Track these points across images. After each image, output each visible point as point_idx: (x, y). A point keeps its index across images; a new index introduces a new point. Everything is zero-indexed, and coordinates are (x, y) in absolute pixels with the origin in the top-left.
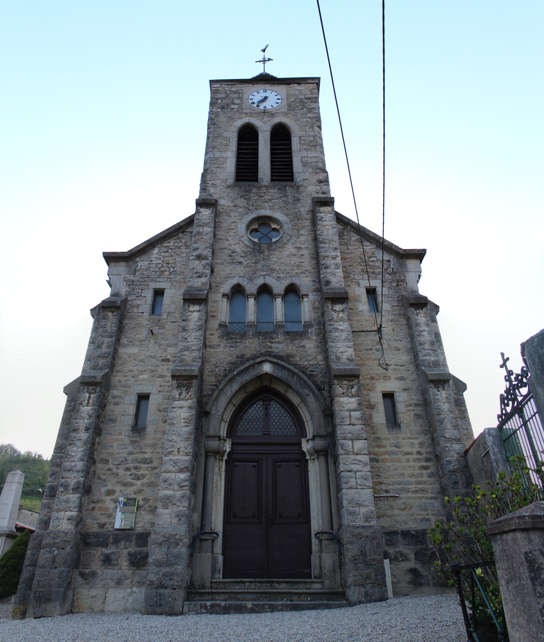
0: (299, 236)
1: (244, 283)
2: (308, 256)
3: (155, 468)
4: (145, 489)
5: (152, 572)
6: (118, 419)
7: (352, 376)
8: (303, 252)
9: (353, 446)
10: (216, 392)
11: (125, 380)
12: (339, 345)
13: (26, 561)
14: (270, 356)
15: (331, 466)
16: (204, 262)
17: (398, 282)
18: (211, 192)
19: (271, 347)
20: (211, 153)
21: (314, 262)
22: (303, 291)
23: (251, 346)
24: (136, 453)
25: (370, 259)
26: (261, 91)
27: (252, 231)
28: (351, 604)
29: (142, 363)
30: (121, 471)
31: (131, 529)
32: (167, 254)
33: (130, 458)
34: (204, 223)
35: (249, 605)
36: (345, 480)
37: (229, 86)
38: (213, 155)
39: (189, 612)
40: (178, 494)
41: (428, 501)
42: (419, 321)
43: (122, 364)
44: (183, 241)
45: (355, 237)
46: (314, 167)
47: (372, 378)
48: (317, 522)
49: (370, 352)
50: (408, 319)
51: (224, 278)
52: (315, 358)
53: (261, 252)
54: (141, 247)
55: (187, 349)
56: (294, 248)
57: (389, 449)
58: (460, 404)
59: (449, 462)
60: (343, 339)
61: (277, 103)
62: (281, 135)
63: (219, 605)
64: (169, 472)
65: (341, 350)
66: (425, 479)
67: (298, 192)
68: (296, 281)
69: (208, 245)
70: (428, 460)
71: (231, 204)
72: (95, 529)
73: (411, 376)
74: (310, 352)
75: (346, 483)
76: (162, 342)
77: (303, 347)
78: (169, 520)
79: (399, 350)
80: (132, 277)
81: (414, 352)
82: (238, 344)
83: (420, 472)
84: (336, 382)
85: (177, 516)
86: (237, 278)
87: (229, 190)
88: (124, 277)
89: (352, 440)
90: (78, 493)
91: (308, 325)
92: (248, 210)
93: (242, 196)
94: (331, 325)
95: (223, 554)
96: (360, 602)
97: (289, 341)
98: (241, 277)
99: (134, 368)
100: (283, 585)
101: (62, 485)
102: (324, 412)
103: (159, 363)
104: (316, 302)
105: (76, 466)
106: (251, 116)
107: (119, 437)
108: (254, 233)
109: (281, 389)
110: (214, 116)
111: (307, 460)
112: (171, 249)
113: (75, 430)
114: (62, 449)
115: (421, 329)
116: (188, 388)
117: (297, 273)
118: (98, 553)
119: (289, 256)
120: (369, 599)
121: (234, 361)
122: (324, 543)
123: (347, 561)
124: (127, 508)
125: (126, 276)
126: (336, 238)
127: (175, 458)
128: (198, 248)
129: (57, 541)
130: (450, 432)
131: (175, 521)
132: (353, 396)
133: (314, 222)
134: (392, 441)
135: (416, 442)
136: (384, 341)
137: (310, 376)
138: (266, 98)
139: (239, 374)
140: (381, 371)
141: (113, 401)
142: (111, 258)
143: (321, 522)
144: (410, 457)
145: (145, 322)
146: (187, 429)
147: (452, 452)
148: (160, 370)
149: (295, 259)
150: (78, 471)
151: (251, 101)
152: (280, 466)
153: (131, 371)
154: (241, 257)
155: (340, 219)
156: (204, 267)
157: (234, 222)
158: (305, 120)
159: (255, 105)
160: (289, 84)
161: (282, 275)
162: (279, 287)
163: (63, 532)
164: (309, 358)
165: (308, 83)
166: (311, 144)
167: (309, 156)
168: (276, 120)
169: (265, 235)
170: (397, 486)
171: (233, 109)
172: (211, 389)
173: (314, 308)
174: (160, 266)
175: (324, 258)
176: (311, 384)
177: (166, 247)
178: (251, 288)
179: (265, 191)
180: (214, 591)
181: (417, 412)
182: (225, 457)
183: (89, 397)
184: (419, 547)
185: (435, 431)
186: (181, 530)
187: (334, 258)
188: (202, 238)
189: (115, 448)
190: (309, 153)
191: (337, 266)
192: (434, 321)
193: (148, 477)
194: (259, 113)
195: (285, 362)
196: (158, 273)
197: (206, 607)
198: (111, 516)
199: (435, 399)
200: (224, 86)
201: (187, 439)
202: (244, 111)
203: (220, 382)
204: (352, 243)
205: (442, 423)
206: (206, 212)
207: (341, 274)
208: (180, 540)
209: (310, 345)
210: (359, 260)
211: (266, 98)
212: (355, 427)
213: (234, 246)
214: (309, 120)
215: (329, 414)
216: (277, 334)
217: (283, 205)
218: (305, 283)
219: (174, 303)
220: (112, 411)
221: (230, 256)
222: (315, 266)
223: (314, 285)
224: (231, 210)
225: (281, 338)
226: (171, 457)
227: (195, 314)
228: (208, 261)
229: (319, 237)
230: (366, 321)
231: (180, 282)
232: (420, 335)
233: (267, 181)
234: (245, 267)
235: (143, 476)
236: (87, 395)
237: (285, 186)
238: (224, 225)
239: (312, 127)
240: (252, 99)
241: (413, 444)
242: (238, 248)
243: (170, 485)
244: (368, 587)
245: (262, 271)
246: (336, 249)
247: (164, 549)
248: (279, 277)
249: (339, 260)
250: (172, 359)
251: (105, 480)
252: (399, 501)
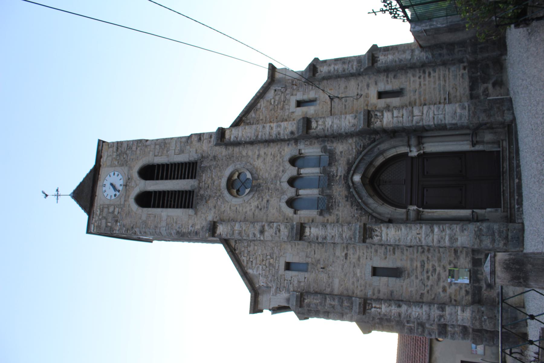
0: (248, 156)
1: (286, 197)
2: (266, 149)
3: (428, 258)
4: (442, 264)
5: (498, 245)
6: (391, 289)
7: (369, 115)
8: (262, 152)
9: (417, 116)
10: (374, 214)
11: (361, 287)
12: (343, 124)
13: (489, 265)
14: (347, 177)
15: (429, 134)
16: (266, 228)
17: (293, 85)
18: (199, 228)
19: (341, 176)
20: (161, 229)
21: (272, 144)
22: (295, 153)
23: (339, 191)
24: (417, 273)
25: (272, 103)
26: (104, 189)
27: (238, 194)
28: (514, 119)
29: (347, 275)
30: (429, 283)
31: (470, 271)
32: (254, 262)
33: (420, 278)
34: (231, 229)
35: (517, 181)
36: (440, 121)
37: (94, 216)
38: (164, 227)
39: (521, 219)
40: (448, 232)
41: (451, 74)
42: (327, 71)
43: (347, 290)
44: (243, 249)
45: (252, 114)
46: (186, 144)
47: (367, 105)
48: (464, 146)
49: (347, 106)
50: (324, 78)
51: (280, 213)
52: (351, 144)
53: (259, 185)
54: (247, 282)
55: (341, 235)
56: (258, 159)
57: (417, 96)
58: (387, 49)
59: (427, 57)
60: (339, 122)
61: (118, 175)
62: (148, 172)
63: (517, 200)
64: (433, 240)
65: (348, 124)
66: (436, 74)
67: (207, 157)
68: (287, 158)
69: (252, 225)
70: (424, 72)
71: (212, 212)
72: (469, 298)
73: (364, 80)
74: (346, 148)
75: (441, 121)
76: (331, 260)
77: (341, 152)
78: (465, 237)
79: (346, 87)
80: (273, 290)
81: (348, 76)
82: (337, 201)
83: (432, 77)
84: (372, 126)
85: (463, 231)
86: (281, 203)
87: (199, 213)
88: (273, 295)
89: (413, 116)
90: (445, 307)
91: (324, 149)
92: (221, 196)
93: (206, 202)
94: (328, 130)
95: (485, 209)
96: (513, 114)
97: (336, 163)
98: (280, 200)
99: (351, 282)
100: (505, 165)
101: (439, 320)
102: (391, 138)
103: (348, 262)
104: (306, 143)
105: (426, 311)
106: (129, 197)
107: (404, 287)
108: (239, 193)
109: (372, 170)
110: (124, 229)
111: (424, 152)
112: (250, 258)
113: (400, 315)
114: (412, 329)
115: (332, 70)
116: (372, 230)
117: (280, 158)
118: (485, 293)
119: (264, 163)
120: (511, 108)
121: (350, 203)
122: (478, 139)
123: (489, 121)
124: (455, 276)
125: (271, 294)
126: (254, 127)
127: (423, 236)
128: (254, 233)
129: (478, 317)
130: (407, 56)
131: (466, 233)
132: (383, 115)
133: (237, 144)
134: (412, 94)
135: (412, 79)
136: (340, 96)
137: (364, 148)
138: (112, 184)
139: (361, 199)
140: (362, 99)
141: (376, 294)
142: (255, 308)
143: (465, 142)
144: (422, 83)
145: (313, 275)
146: (403, 229)
147: (421, 56)
148: (354, 260)
149: (268, 159)
150: (430, 309)
151: (113, 197)
152: (427, 173)
153: (353, 283)
154: (262, 201)
155: (237, 123)
156: (272, 227)
157: (230, 208)
158: (138, 152)
159: (118, 194)
160: (100, 166)
161: (281, 168)
162: (292, 171)
163: (472, 314)
164: (350, 148)
165: (102, 150)
166: (163, 147)
167: (174, 148)
168: (135, 175)
169: (243, 184)
170: (442, 92)
171: (118, 213)
172: (372, 219)
173: (311, 144)
174: (264, 267)
175: (271, 136)
176: (370, 147)
177: (247, 263)
178: (291, 192)
179: (203, 183)
180: (509, 207)
181: (392, 77)
182: (421, 209)
183: (375, 307)
184: (479, 81)
185: (406, 65)
186: (472, 227)
187: (272, 128)
188: (245, 230)
189: (412, 289)
190: (171, 148)
191: (279, 126)
192: (325, 61)
193: (434, 263)
194: (126, 191)
195: (352, 166)
196: (271, 268)
197: (519, 208)
198: (461, 287)
199: (385, 63)
200: (93, 221)
201: (411, 228)
202: (122, 203)
203: (366, 212)
204: (258, 116)
205: (401, 60)
206: (221, 229)
207: (286, 123)
208: (478, 228)
209: (340, 148)
210: (273, 112)
211: (112, 184)
212: (405, 114)
213: (252, 207)
214: (139, 148)
215: (393, 133)
216: (331, 171)
217: (218, 169)
218: (289, 151)
219: (298, 253)
220: (385, 294)
221: (261, 209)
222: (275, 144)
223: (292, 145)
224: (219, 210)
225: (333, 169)
226: (423, 239)
227: (311, 232)
228: (266, 225)
229: (252, 140)
230: (323, 108)
231: (280, 249)
232: (337, 71)
233: (194, 182)
234: (272, 198)
235: (433, 266)
236: (373, 310)
237: (200, 168)
238: (232, 215)
239: (146, 146)
240: (111, 196)
241: (414, 81)
242: (254, 203)
243: (442, 238)
244: (504, 108)
245: (276, 185)
246: (264, 127)
247: (484, 238)
248: (283, 171)
249: (274, 125)
250: (346, 251)
251: (436, 294)
252: (451, 92)
